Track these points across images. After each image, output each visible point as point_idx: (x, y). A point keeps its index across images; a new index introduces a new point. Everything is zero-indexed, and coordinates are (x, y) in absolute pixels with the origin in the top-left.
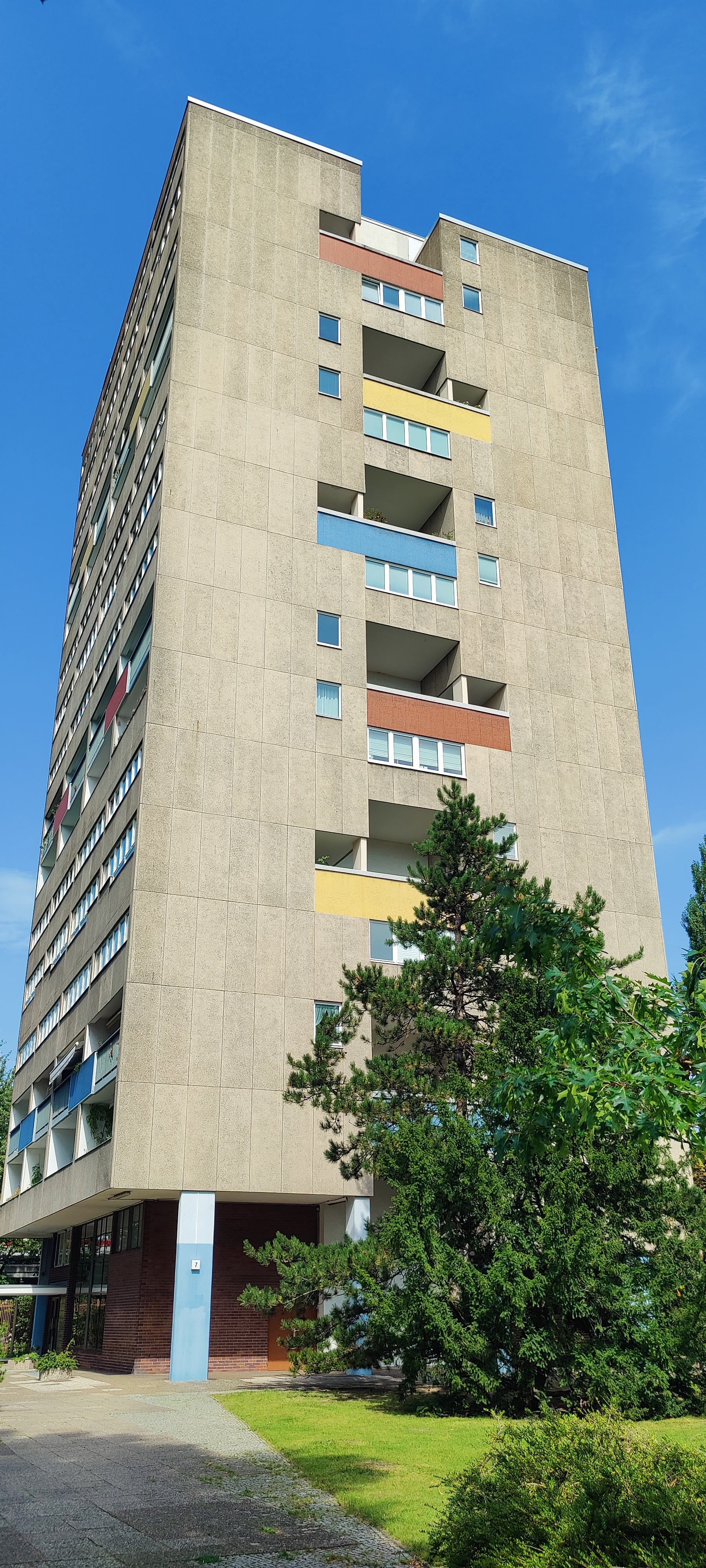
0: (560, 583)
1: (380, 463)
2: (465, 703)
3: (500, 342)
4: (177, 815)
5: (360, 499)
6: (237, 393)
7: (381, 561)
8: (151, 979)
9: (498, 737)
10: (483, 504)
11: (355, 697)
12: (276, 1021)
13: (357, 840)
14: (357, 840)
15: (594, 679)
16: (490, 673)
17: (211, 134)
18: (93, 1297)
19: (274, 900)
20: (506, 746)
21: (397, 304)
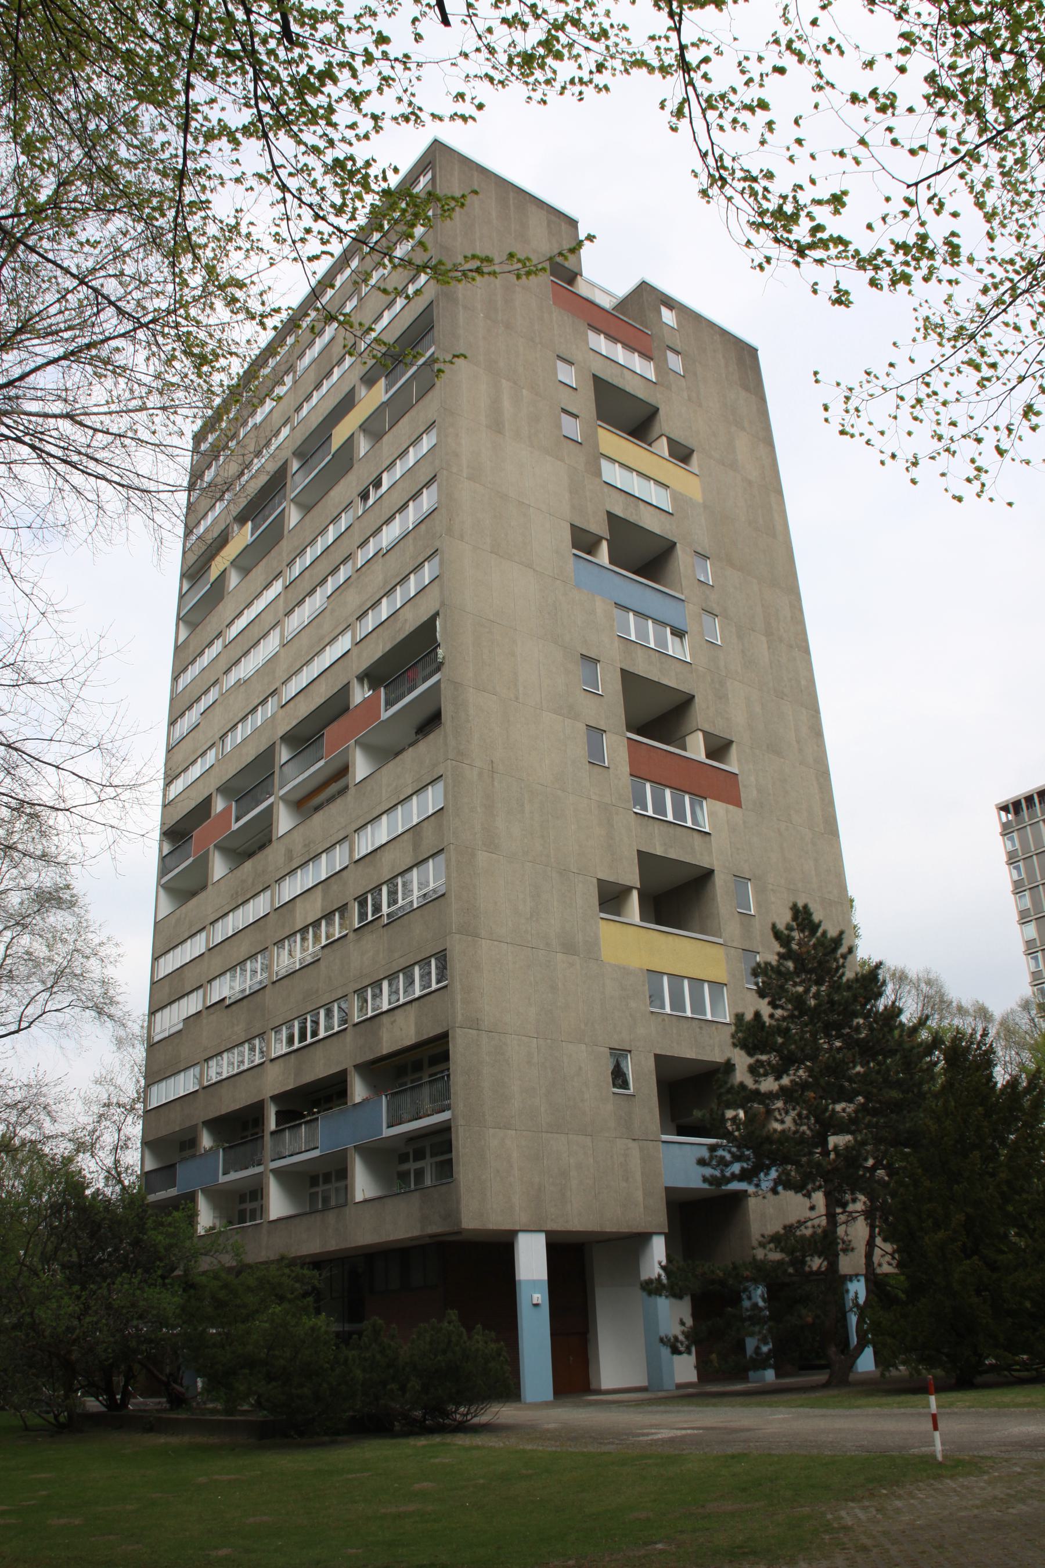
0: (765, 646)
1: (618, 511)
2: (702, 756)
3: (700, 406)
4: (482, 857)
5: (604, 545)
6: (497, 426)
7: (627, 609)
8: (475, 1024)
9: (728, 790)
10: (662, 106)
11: (616, 746)
12: (580, 1068)
13: (629, 889)
14: (629, 889)
15: (798, 742)
16: (719, 729)
17: (456, 173)
18: (782, 1122)
19: (569, 948)
20: (738, 804)
21: (667, 649)
